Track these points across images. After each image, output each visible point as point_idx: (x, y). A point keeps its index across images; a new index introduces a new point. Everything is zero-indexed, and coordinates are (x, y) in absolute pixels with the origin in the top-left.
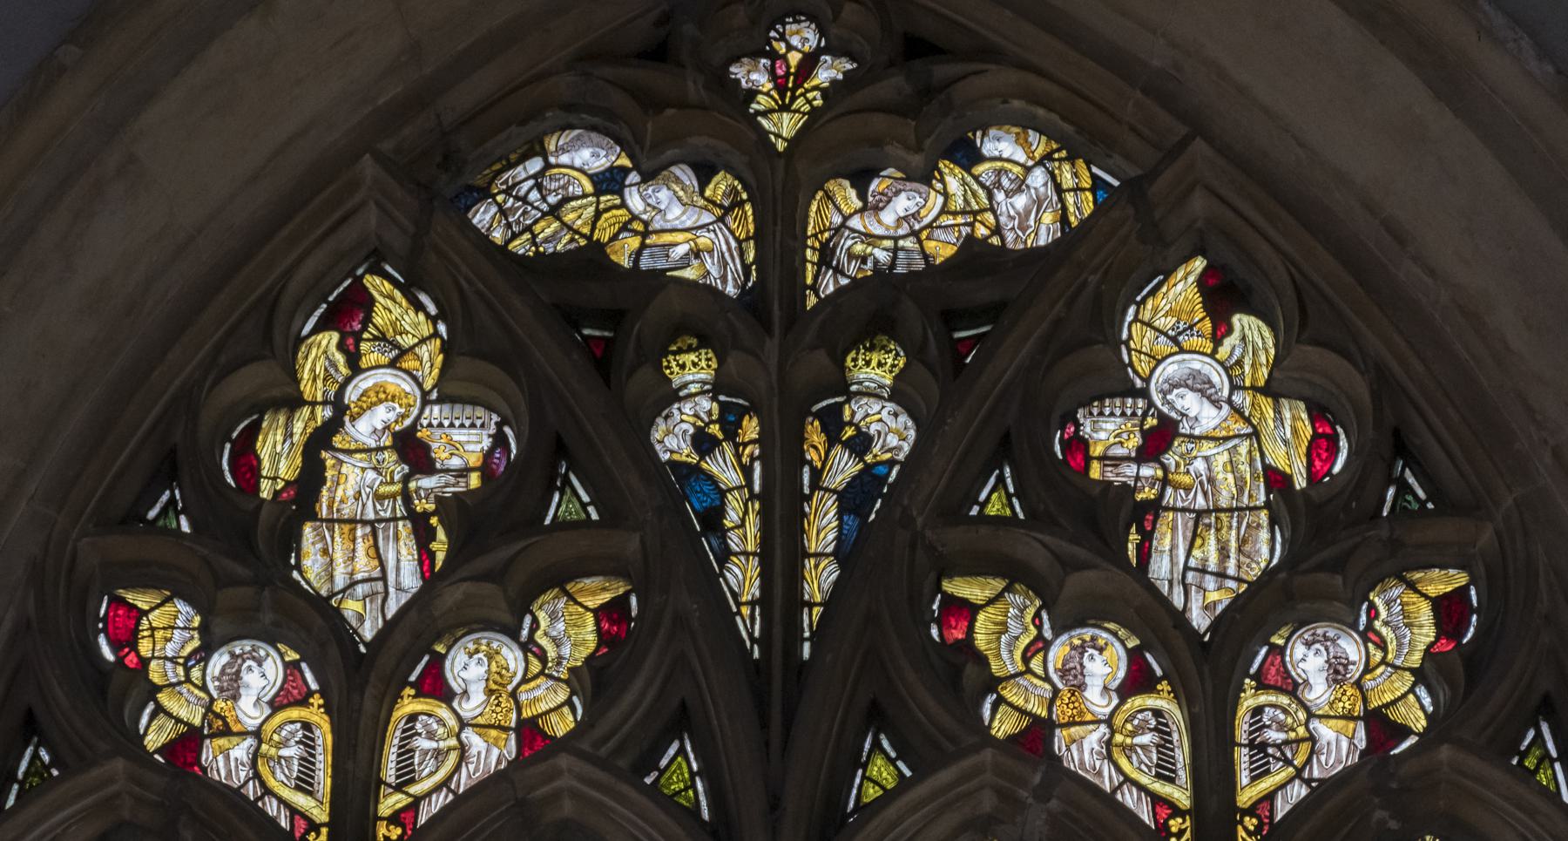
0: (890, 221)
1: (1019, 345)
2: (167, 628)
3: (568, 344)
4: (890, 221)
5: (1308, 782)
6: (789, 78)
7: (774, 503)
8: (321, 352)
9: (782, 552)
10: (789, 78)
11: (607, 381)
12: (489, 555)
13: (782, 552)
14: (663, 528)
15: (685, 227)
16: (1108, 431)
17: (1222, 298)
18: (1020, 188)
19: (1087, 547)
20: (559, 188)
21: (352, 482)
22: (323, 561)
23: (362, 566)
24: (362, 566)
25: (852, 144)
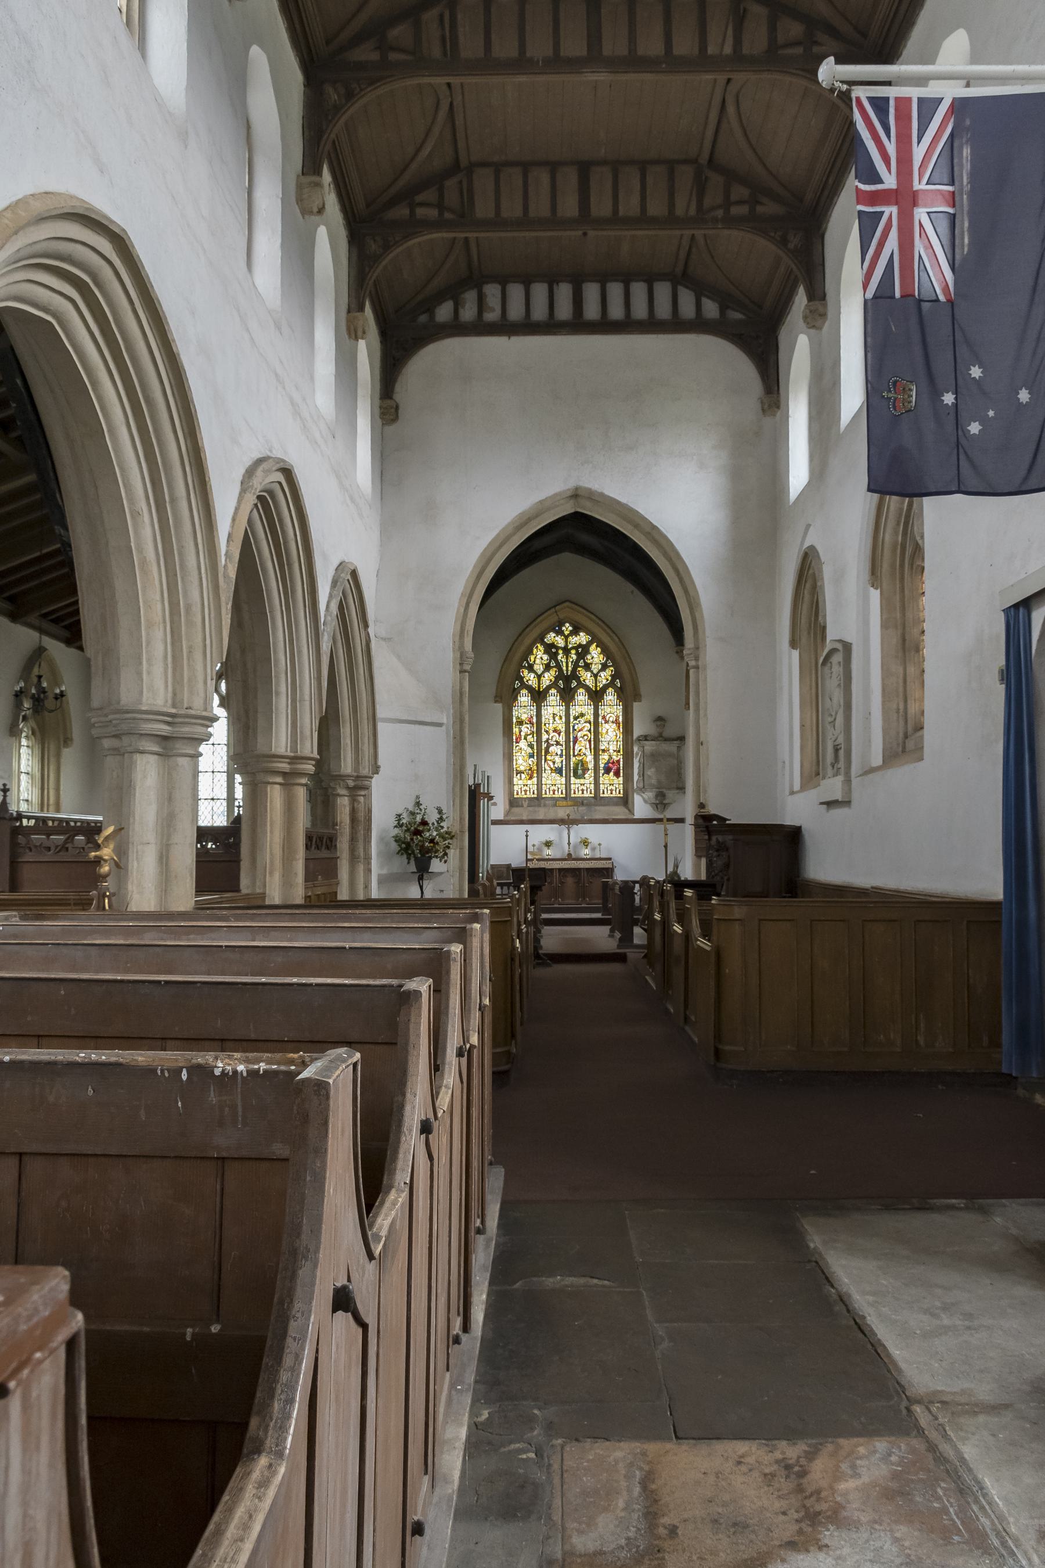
0: (574, 640)
1: (583, 651)
2: (526, 672)
3: (551, 650)
4: (574, 640)
5: (604, 751)
6: (567, 628)
7: (566, 663)
8: (535, 650)
9: (567, 666)
10: (567, 628)
11: (388, 408)
12: (548, 667)
13: (567, 666)
14: (558, 666)
15: (560, 641)
16: (589, 657)
17: (597, 646)
18: (583, 638)
19: (587, 667)
20: (551, 638)
21: (538, 661)
22: (536, 667)
23: (539, 668)
24: (539, 668)
25: (572, 633)
